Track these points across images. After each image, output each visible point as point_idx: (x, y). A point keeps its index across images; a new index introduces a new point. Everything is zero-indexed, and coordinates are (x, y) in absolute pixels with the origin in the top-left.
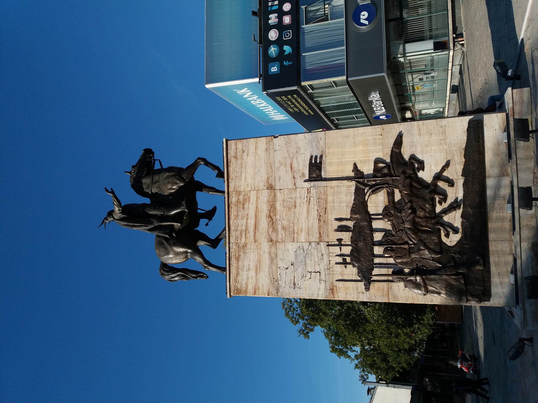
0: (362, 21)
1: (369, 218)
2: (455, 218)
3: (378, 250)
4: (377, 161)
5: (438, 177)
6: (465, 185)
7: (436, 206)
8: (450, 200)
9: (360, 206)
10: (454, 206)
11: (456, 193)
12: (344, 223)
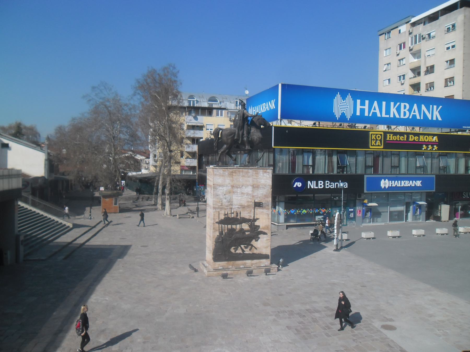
0: (296, 183)
1: (240, 223)
2: (239, 251)
3: (230, 226)
4: (259, 226)
5: (252, 246)
6: (249, 254)
7: (67, 331)
8: (245, 249)
9: (244, 220)
10: (243, 251)
11: (247, 251)
12: (239, 214)
